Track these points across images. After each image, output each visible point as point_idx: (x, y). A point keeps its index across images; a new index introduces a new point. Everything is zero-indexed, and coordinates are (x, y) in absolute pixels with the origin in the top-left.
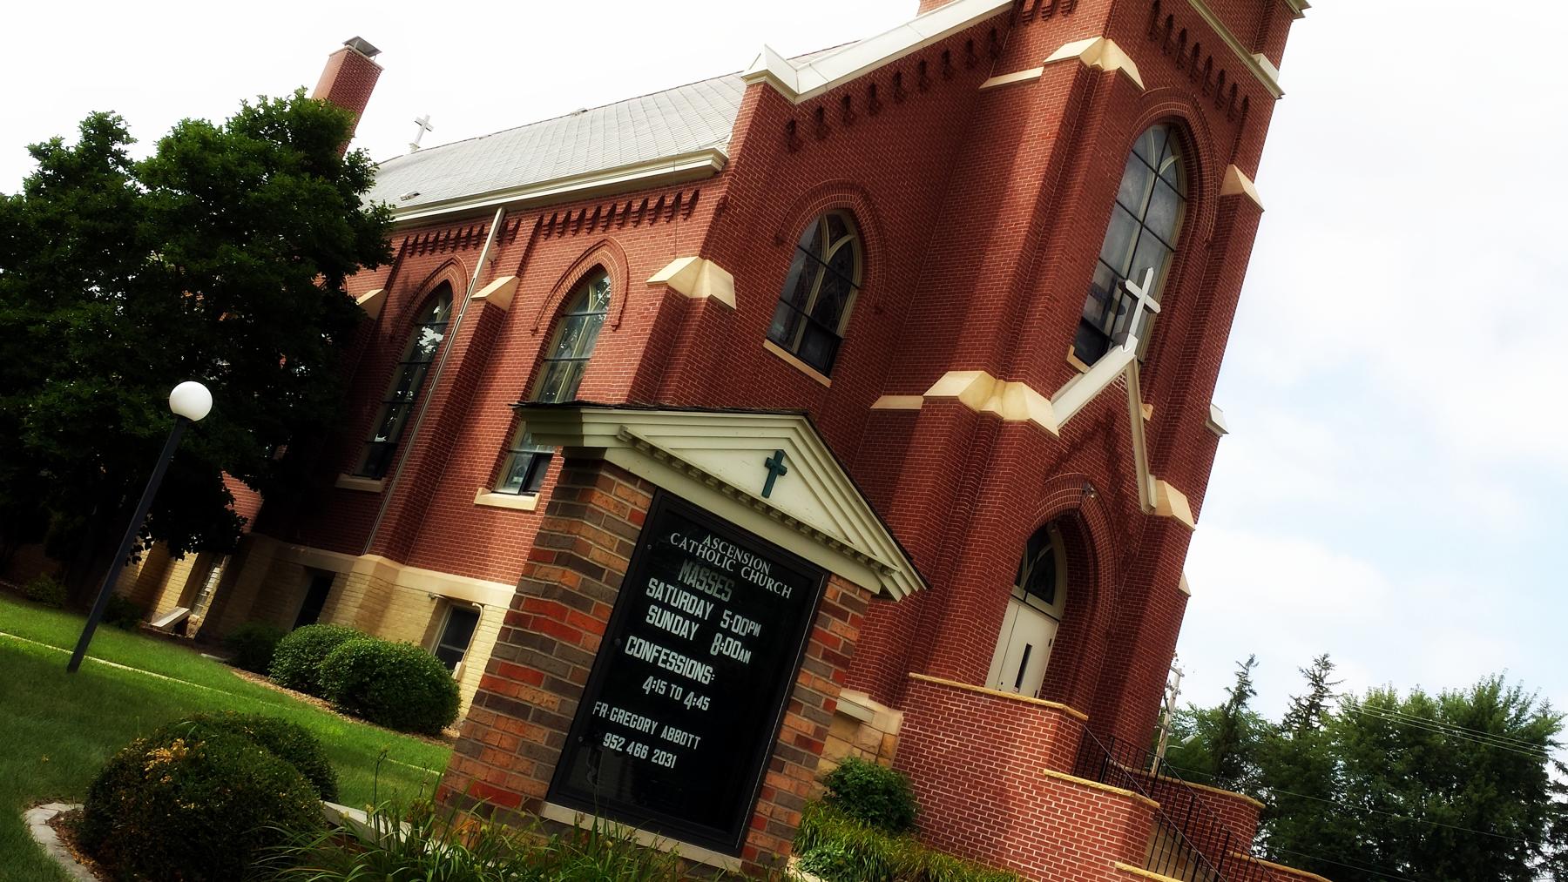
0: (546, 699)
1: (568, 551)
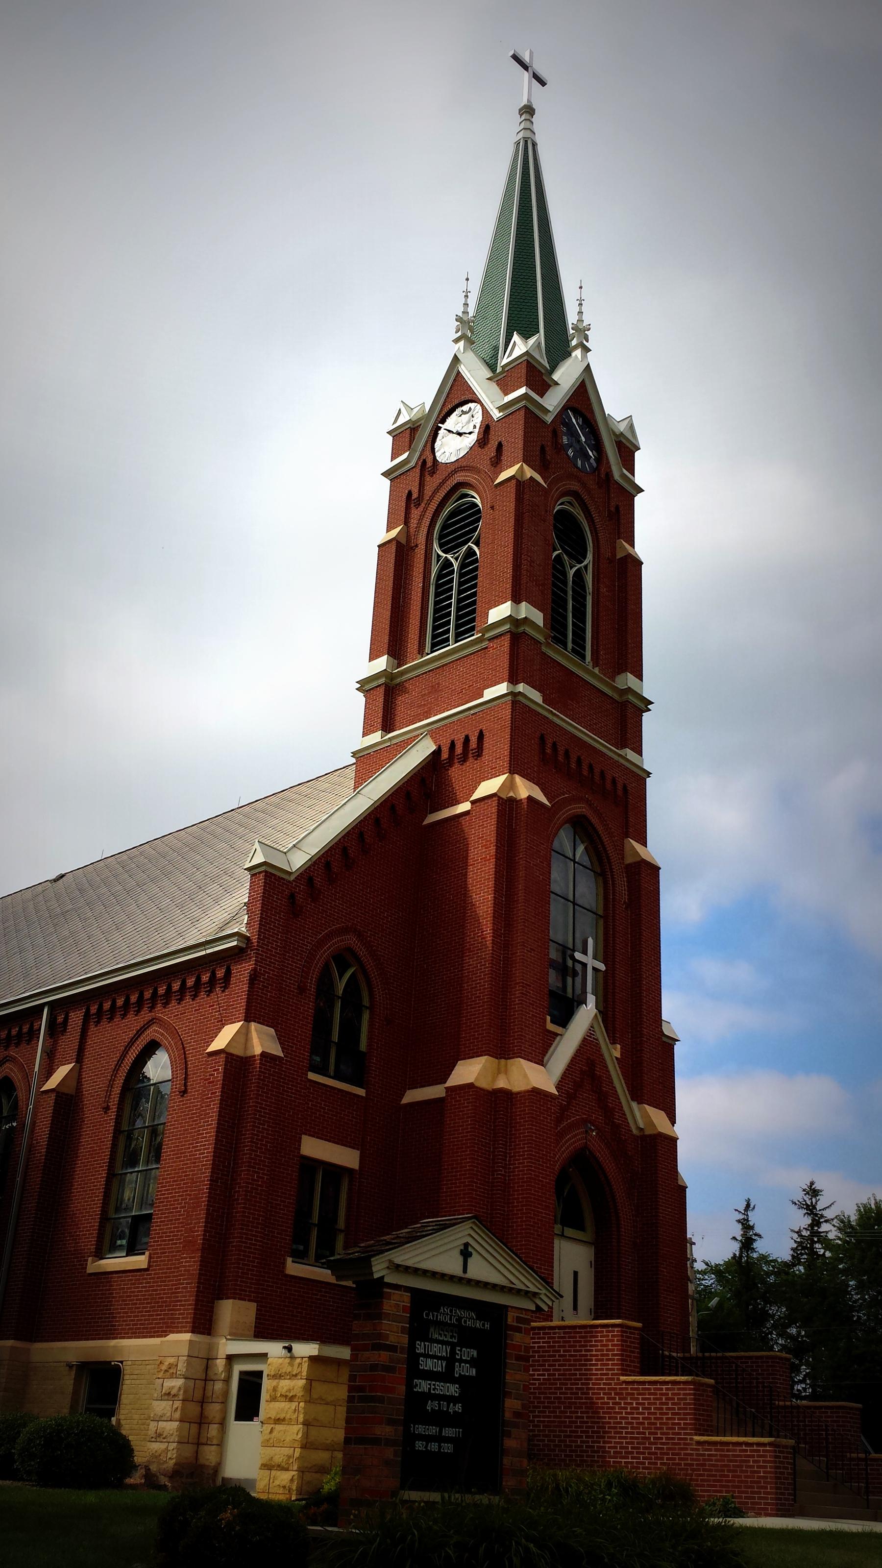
0: (385, 1431)
1: (378, 1341)
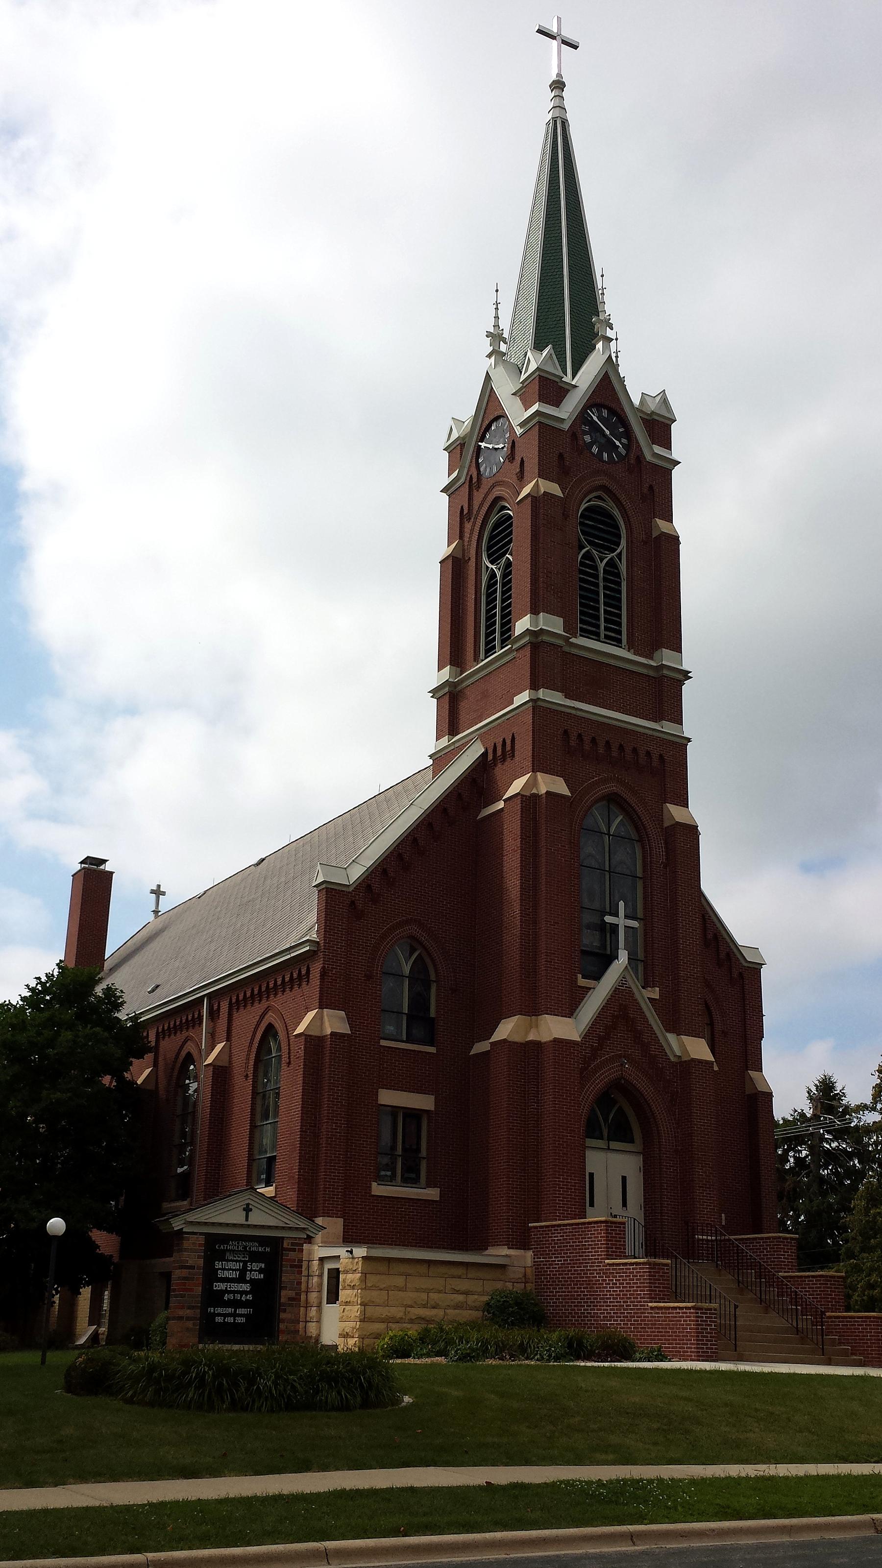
0: (188, 1312)
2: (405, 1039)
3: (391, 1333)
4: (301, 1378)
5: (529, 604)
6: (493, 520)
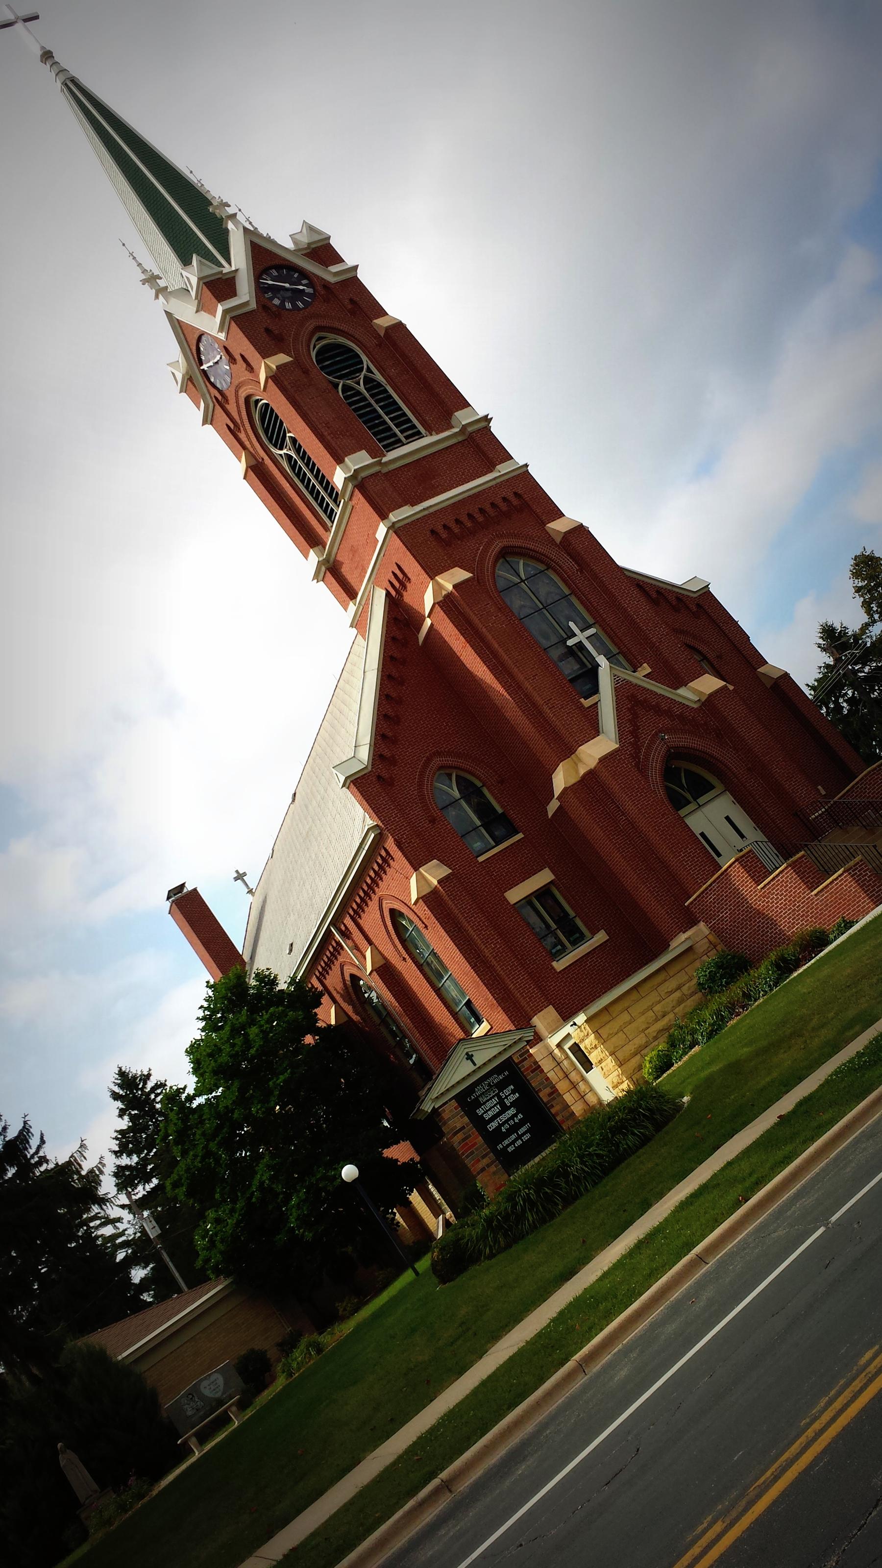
0: (485, 1162)
2: (494, 844)
3: (647, 1058)
4: (598, 1144)
5: (331, 459)
6: (257, 417)
